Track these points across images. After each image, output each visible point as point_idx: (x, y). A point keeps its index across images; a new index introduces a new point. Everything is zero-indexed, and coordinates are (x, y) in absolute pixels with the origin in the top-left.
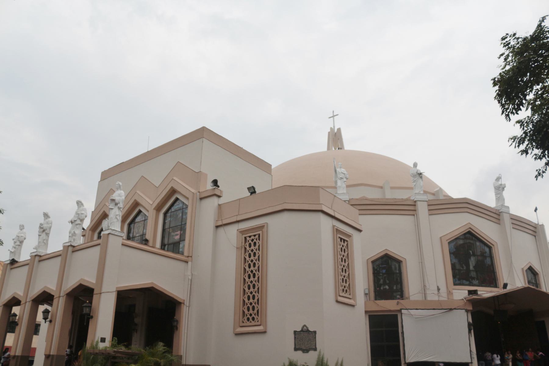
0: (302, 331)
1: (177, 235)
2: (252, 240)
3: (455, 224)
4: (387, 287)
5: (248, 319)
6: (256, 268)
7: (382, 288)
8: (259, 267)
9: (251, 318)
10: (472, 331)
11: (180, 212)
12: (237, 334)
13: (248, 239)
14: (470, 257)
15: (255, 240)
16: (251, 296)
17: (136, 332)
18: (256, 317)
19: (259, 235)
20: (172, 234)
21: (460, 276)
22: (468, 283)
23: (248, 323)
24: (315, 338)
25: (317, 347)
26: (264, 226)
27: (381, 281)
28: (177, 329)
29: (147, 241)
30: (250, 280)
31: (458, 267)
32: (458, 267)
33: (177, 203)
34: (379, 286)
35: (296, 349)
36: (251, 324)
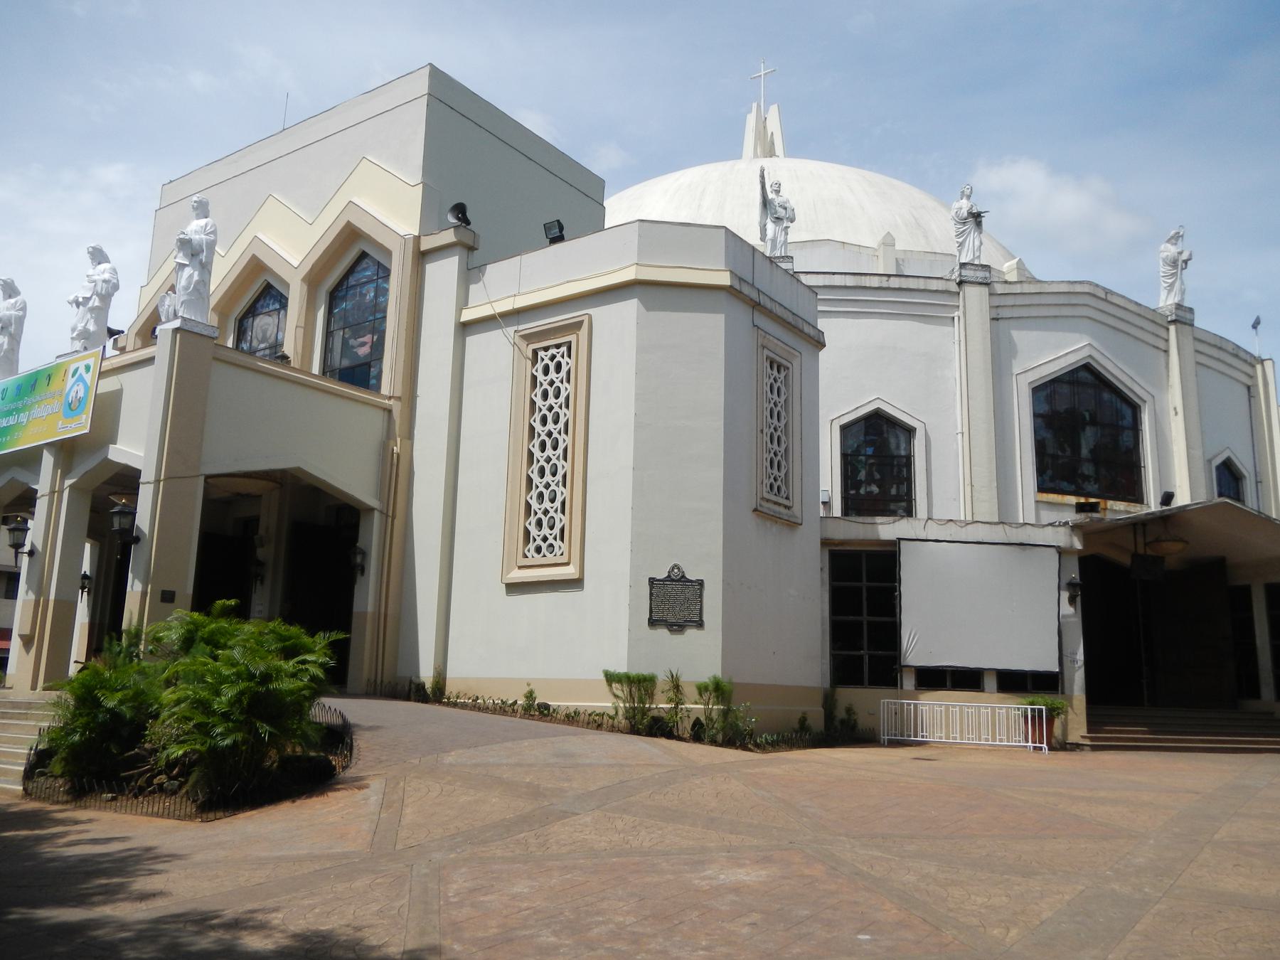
1: (363, 344)
2: (553, 358)
3: (1049, 352)
4: (875, 489)
5: (538, 550)
6: (561, 425)
7: (862, 491)
8: (569, 372)
9: (544, 546)
10: (1079, 599)
11: (372, 286)
12: (514, 588)
13: (541, 354)
14: (1084, 431)
15: (558, 358)
16: (552, 366)
17: (262, 583)
18: (557, 544)
19: (570, 342)
20: (352, 342)
21: (1055, 472)
22: (1073, 487)
23: (538, 559)
24: (701, 596)
25: (705, 618)
26: (582, 322)
27: (862, 475)
29: (285, 358)
32: (1050, 450)
34: (857, 485)
35: (653, 623)
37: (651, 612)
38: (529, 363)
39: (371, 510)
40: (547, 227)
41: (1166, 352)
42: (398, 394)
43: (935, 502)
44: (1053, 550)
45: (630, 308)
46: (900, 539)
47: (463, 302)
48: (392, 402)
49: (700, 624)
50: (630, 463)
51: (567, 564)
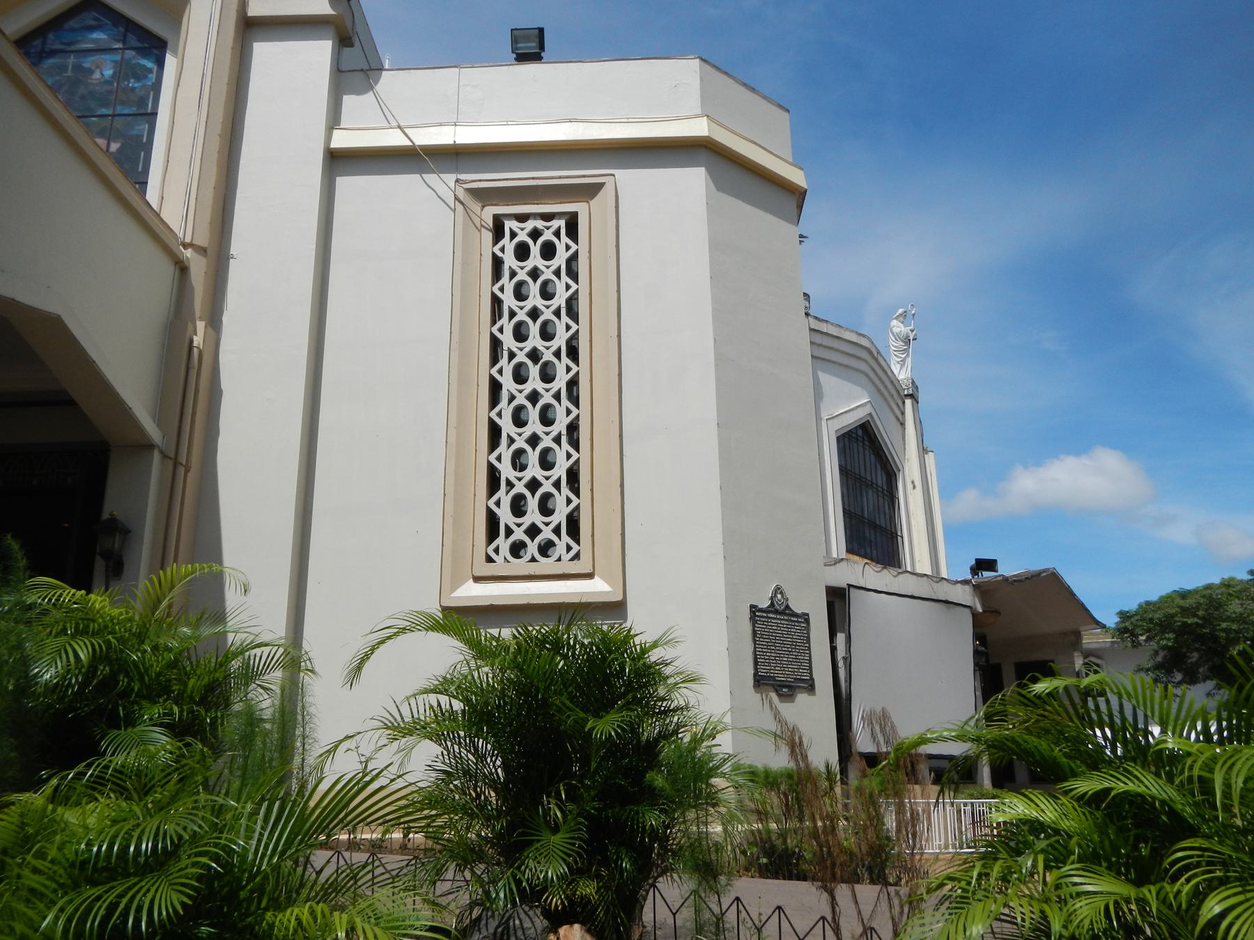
2: (535, 234)
13: (509, 225)
35: (760, 682)
37: (756, 663)
38: (488, 236)
39: (150, 446)
40: (517, 36)
41: (903, 424)
42: (202, 241)
43: (560, 572)
44: (967, 611)
45: (692, 180)
46: (849, 586)
47: (334, 120)
48: (188, 253)
49: (811, 687)
50: (712, 415)
51: (590, 576)
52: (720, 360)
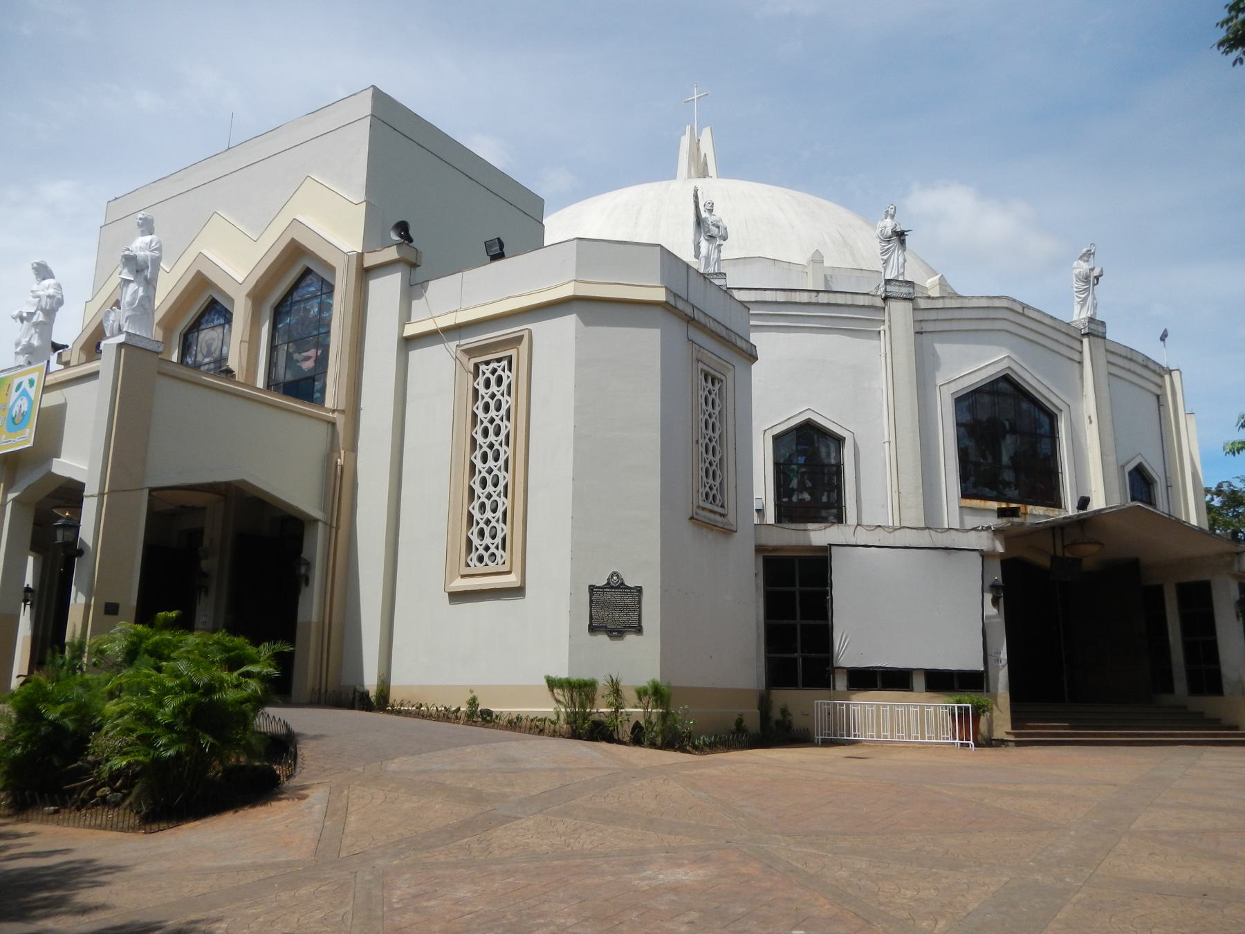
0: (608, 585)
1: (307, 358)
3: (971, 364)
4: (807, 496)
5: (481, 559)
6: (502, 437)
7: (794, 499)
9: (486, 555)
10: (1002, 600)
12: (457, 597)
13: (483, 367)
14: (1004, 439)
15: (499, 372)
17: (206, 593)
18: (499, 553)
19: (510, 359)
20: (296, 356)
21: (976, 480)
22: (994, 493)
23: (480, 568)
24: (639, 602)
25: (644, 624)
27: (794, 483)
28: (307, 583)
29: (229, 372)
30: (487, 466)
31: (974, 456)
32: (974, 456)
33: (308, 280)
34: (789, 494)
35: (593, 629)
36: (487, 570)
37: (591, 618)
39: (316, 521)
40: (488, 245)
44: (977, 554)
45: (568, 323)
47: (406, 317)
48: (335, 415)
49: (639, 630)
51: (509, 572)
52: (578, 438)
